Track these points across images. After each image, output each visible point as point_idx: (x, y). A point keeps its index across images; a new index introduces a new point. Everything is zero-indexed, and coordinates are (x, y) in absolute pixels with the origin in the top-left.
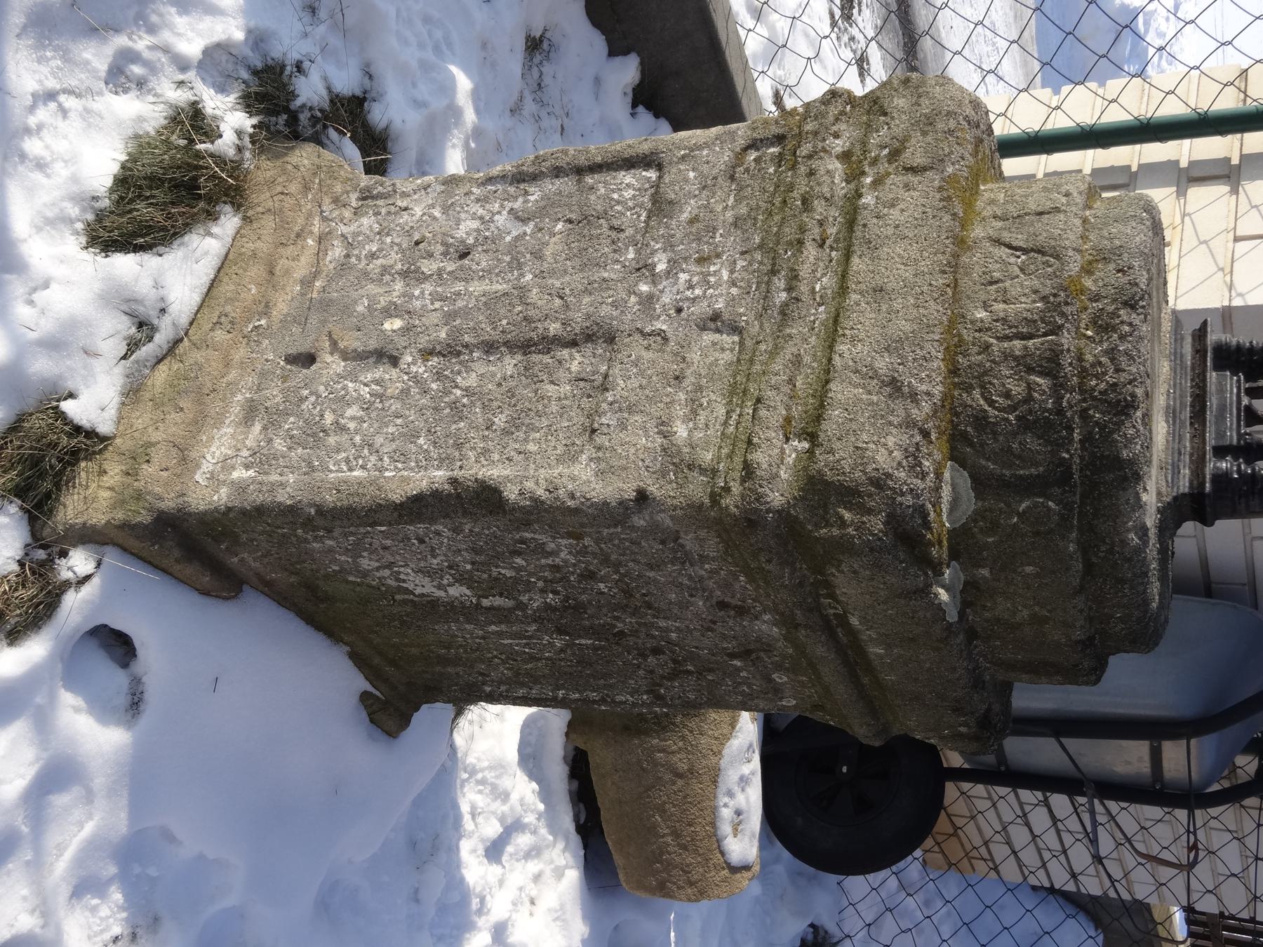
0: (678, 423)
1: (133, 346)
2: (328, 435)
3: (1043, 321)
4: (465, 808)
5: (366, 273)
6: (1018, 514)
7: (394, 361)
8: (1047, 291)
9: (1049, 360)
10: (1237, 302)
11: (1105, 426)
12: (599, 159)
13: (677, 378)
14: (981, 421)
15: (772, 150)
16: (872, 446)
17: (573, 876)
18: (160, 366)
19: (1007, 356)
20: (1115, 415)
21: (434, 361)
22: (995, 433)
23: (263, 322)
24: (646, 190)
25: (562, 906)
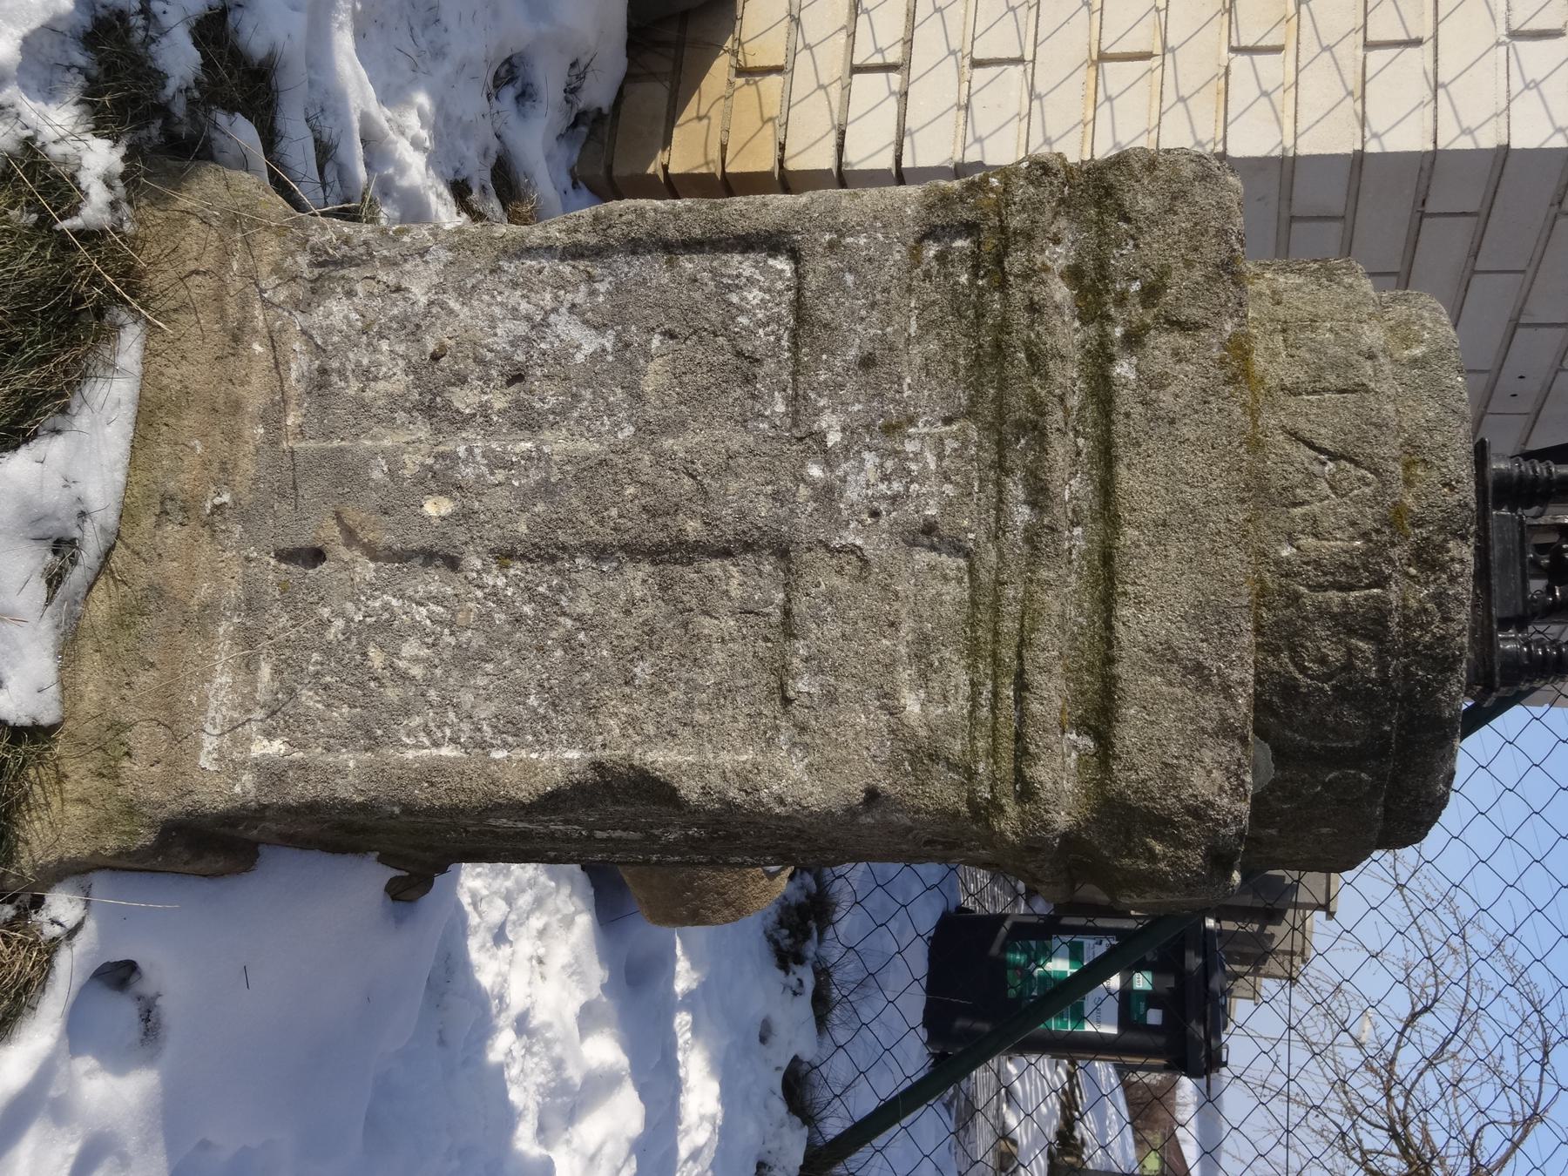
0: (905, 691)
1: (54, 580)
2: (382, 685)
3: (1366, 570)
4: (465, 900)
5: (364, 407)
6: (1324, 784)
7: (453, 563)
8: (1369, 524)
9: (1375, 621)
10: (1373, 147)
11: (1428, 685)
12: (697, 232)
13: (892, 624)
14: (1289, 690)
15: (959, 243)
16: (1184, 762)
17: (584, 921)
18: (94, 594)
19: (1323, 612)
20: (1441, 672)
21: (516, 569)
22: (1306, 704)
23: (226, 498)
24: (780, 293)
25: (577, 958)
